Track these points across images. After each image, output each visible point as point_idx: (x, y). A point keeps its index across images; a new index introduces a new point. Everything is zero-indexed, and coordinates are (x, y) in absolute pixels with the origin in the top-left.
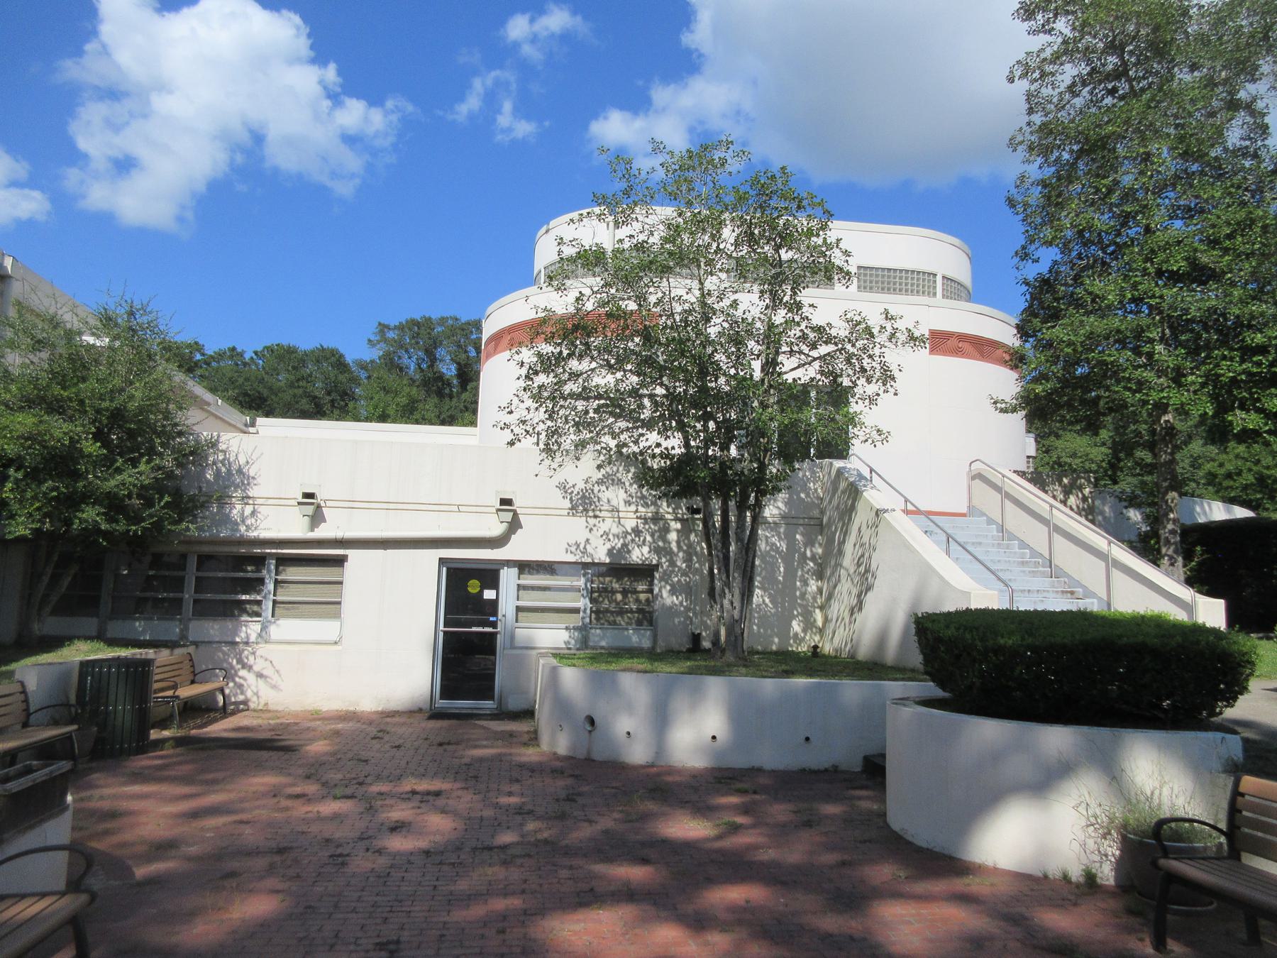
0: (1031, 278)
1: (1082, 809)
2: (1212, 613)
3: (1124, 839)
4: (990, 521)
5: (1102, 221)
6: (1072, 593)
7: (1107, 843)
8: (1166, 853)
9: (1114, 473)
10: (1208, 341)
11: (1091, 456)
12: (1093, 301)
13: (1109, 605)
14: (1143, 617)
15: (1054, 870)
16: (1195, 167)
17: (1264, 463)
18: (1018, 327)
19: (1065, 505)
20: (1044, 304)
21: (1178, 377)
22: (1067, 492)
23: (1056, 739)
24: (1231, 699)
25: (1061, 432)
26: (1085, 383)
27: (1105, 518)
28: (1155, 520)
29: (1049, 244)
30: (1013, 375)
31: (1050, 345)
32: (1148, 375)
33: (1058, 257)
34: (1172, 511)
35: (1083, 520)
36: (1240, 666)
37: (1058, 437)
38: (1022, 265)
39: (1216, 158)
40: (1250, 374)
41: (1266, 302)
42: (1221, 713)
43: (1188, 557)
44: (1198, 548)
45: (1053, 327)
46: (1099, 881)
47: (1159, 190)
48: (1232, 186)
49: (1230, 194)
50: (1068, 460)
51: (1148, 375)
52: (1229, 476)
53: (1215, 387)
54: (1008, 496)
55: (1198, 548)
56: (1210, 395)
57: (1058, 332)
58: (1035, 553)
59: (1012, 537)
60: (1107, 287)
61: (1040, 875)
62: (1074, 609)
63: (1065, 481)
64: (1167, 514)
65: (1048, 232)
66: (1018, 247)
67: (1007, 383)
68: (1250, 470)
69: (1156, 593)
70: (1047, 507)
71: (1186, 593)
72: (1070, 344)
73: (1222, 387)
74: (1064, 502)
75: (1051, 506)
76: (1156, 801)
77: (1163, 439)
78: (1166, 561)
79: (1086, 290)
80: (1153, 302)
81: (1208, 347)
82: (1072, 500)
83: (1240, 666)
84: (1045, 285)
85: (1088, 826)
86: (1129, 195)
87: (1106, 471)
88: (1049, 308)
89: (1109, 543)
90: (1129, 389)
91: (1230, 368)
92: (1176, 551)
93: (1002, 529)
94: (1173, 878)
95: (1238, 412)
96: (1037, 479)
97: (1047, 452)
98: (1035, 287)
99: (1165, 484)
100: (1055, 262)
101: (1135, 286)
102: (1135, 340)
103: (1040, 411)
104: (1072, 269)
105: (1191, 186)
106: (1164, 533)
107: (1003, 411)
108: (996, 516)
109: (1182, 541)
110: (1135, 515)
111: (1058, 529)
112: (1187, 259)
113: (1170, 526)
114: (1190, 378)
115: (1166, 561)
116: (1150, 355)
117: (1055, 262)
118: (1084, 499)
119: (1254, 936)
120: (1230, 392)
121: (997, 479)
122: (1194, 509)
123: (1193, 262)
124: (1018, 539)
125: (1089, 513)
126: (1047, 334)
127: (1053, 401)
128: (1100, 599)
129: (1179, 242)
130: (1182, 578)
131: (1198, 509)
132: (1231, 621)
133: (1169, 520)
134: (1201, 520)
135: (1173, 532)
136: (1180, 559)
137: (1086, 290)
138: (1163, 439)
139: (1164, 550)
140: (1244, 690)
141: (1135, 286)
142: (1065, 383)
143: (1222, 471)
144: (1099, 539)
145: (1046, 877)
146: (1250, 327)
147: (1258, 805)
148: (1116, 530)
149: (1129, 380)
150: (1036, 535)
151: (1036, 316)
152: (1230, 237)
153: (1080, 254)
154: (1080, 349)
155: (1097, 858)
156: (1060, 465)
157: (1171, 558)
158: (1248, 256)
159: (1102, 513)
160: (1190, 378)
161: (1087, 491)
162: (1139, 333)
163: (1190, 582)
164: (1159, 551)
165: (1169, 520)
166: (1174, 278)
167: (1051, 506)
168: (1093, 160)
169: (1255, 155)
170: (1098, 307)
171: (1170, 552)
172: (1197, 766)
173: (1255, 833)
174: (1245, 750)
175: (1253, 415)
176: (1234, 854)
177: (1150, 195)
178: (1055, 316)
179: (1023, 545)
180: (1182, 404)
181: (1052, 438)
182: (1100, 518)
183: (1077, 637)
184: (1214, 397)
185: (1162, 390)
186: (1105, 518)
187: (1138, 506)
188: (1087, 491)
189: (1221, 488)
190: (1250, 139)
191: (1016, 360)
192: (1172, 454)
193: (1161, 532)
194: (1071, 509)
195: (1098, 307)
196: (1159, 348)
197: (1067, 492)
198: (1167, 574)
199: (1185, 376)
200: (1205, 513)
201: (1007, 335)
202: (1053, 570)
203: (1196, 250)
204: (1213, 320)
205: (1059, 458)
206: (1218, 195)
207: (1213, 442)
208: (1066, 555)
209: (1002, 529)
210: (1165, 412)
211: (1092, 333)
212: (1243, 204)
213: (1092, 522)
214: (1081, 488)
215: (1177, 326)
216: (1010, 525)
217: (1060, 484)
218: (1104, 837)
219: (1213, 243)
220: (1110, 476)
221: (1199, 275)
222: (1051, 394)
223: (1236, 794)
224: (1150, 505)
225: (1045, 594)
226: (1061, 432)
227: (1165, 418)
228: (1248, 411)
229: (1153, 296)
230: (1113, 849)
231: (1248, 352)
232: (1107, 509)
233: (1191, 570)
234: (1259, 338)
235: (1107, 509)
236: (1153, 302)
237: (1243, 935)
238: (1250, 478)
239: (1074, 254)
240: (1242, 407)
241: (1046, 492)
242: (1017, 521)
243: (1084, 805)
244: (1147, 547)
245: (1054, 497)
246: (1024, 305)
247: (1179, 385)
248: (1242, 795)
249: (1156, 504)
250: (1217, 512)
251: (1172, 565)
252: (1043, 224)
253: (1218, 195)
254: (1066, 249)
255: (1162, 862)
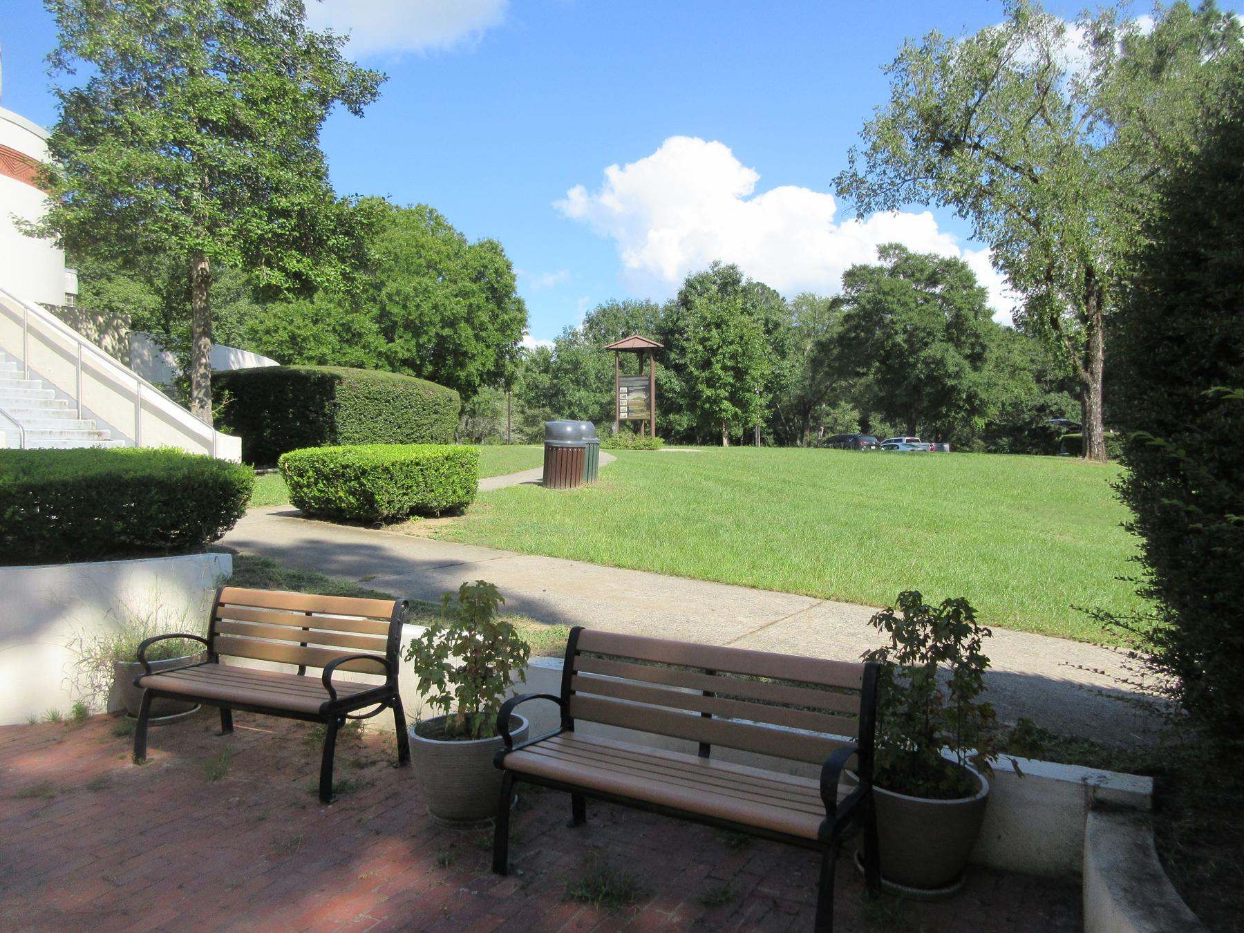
0: (66, 90)
1: (76, 647)
2: (229, 448)
3: (116, 666)
4: (9, 357)
5: (145, 48)
6: (99, 434)
7: (99, 674)
8: (149, 671)
9: (167, 322)
10: (242, 199)
11: (144, 303)
12: (133, 132)
13: (137, 445)
14: (155, 452)
15: (42, 713)
16: (241, 25)
17: (295, 323)
18: (49, 142)
19: (100, 346)
20: (80, 123)
21: (213, 228)
22: (102, 331)
23: (48, 579)
24: (229, 523)
25: (113, 275)
26: (124, 219)
27: (143, 362)
28: (188, 364)
29: (89, 57)
30: (43, 195)
31: (84, 169)
32: (187, 220)
33: (99, 76)
34: (204, 356)
35: (118, 363)
36: (239, 492)
37: (109, 279)
38: (54, 71)
39: (259, 22)
40: (275, 234)
41: (292, 171)
42: (221, 536)
43: (217, 399)
44: (227, 392)
45: (91, 151)
46: (91, 713)
47: (205, 35)
48: (272, 54)
49: (269, 61)
50: (120, 305)
51: (187, 220)
52: (268, 332)
53: (245, 242)
54: (31, 330)
55: (227, 392)
56: (241, 249)
57: (92, 157)
58: (61, 394)
59: (35, 375)
60: (151, 122)
61: (27, 722)
62: (87, 447)
63: (101, 319)
64: (199, 359)
65: (85, 43)
66: (51, 52)
67: (34, 203)
68: (285, 329)
69: (197, 436)
70: (75, 344)
71: (208, 432)
72: (105, 172)
73: (252, 243)
74: (99, 343)
75: (80, 344)
76: (151, 625)
77: (199, 286)
78: (196, 403)
79: (127, 120)
80: (194, 148)
81: (241, 203)
82: (108, 341)
83: (239, 492)
84: (80, 103)
85: (80, 662)
86: (176, 30)
87: (159, 320)
88: (85, 129)
89: (139, 383)
90: (166, 231)
91: (259, 227)
92: (206, 395)
93: (23, 366)
94: (153, 693)
95: (264, 267)
96: (68, 315)
97: (97, 294)
98: (70, 102)
99: (199, 330)
100: (94, 80)
101: (177, 128)
102: (170, 182)
103: (79, 239)
104: (113, 92)
105: (235, 40)
106: (196, 377)
107: (29, 234)
108: (18, 352)
109: (212, 385)
110: (171, 359)
111: (85, 368)
112: (227, 112)
113: (202, 371)
114: (224, 230)
115: (196, 403)
116: (187, 200)
117: (94, 80)
118: (120, 340)
119: (227, 726)
120: (257, 248)
121: (18, 310)
122: (229, 358)
123: (231, 116)
124: (43, 378)
125: (125, 356)
126: (81, 156)
127: (88, 233)
128: (128, 439)
129: (220, 94)
130: (211, 419)
131: (232, 357)
132: (248, 457)
133: (200, 365)
134: (235, 367)
135: (204, 376)
136: (210, 402)
137: (127, 120)
138: (199, 286)
139: (195, 393)
140: (241, 514)
141: (177, 128)
142: (99, 214)
143: (263, 327)
144: (128, 379)
145: (33, 723)
146: (277, 190)
147: (234, 611)
148: (152, 375)
149: (166, 221)
150: (63, 374)
151: (71, 134)
152: (265, 100)
153: (123, 79)
154: (116, 181)
155: (90, 691)
156: (112, 309)
157: (201, 401)
158: (280, 124)
159: (141, 356)
160: (224, 230)
161: (123, 331)
162: (179, 175)
163: (217, 425)
164: (190, 394)
165: (200, 365)
166: (216, 129)
167: (80, 344)
168: (832, 429)
169: (292, 32)
170: (133, 137)
171: (201, 395)
172: (190, 586)
173: (823, 735)
174: (235, 566)
175: (277, 273)
176: (212, 657)
177: (195, 37)
178: (90, 140)
179: (48, 384)
180: (216, 253)
181: (104, 280)
182: (138, 361)
183: (80, 473)
184: (245, 251)
185: (198, 237)
186: (143, 362)
187: (173, 350)
188: (123, 331)
189: (256, 340)
190: (290, 15)
191: (46, 180)
192: (207, 301)
193: (194, 376)
194: (106, 350)
195: (133, 137)
196: (197, 194)
197: (102, 331)
198: (197, 416)
199: (219, 226)
200: (239, 362)
201: (38, 151)
202: (81, 413)
203: (234, 105)
204: (247, 175)
205: (110, 301)
206: (258, 57)
207: (257, 303)
208: (95, 396)
209: (23, 366)
210: (202, 260)
211: (129, 165)
212: (279, 74)
213: (128, 364)
214: (117, 328)
215: (215, 174)
216: (33, 362)
217: (95, 323)
218: (97, 668)
219: (250, 102)
220: (163, 326)
221: (235, 131)
222: (84, 223)
223: (218, 604)
224: (184, 350)
225: (69, 436)
226: (113, 275)
227: (202, 265)
228: (272, 268)
229: (193, 143)
230: (105, 679)
231: (275, 213)
232: (146, 352)
233: (219, 412)
234: (284, 203)
235: (146, 352)
236: (194, 148)
237: (219, 728)
238: (286, 337)
239: (117, 77)
240: (269, 264)
241: (77, 329)
242: (39, 356)
243: (77, 643)
244: (180, 391)
245: (88, 336)
246: (59, 120)
247: (213, 234)
248: (222, 605)
249: (189, 349)
250: (248, 360)
251: (202, 407)
252: (81, 32)
253: (258, 57)
254: (106, 67)
255: (146, 681)
